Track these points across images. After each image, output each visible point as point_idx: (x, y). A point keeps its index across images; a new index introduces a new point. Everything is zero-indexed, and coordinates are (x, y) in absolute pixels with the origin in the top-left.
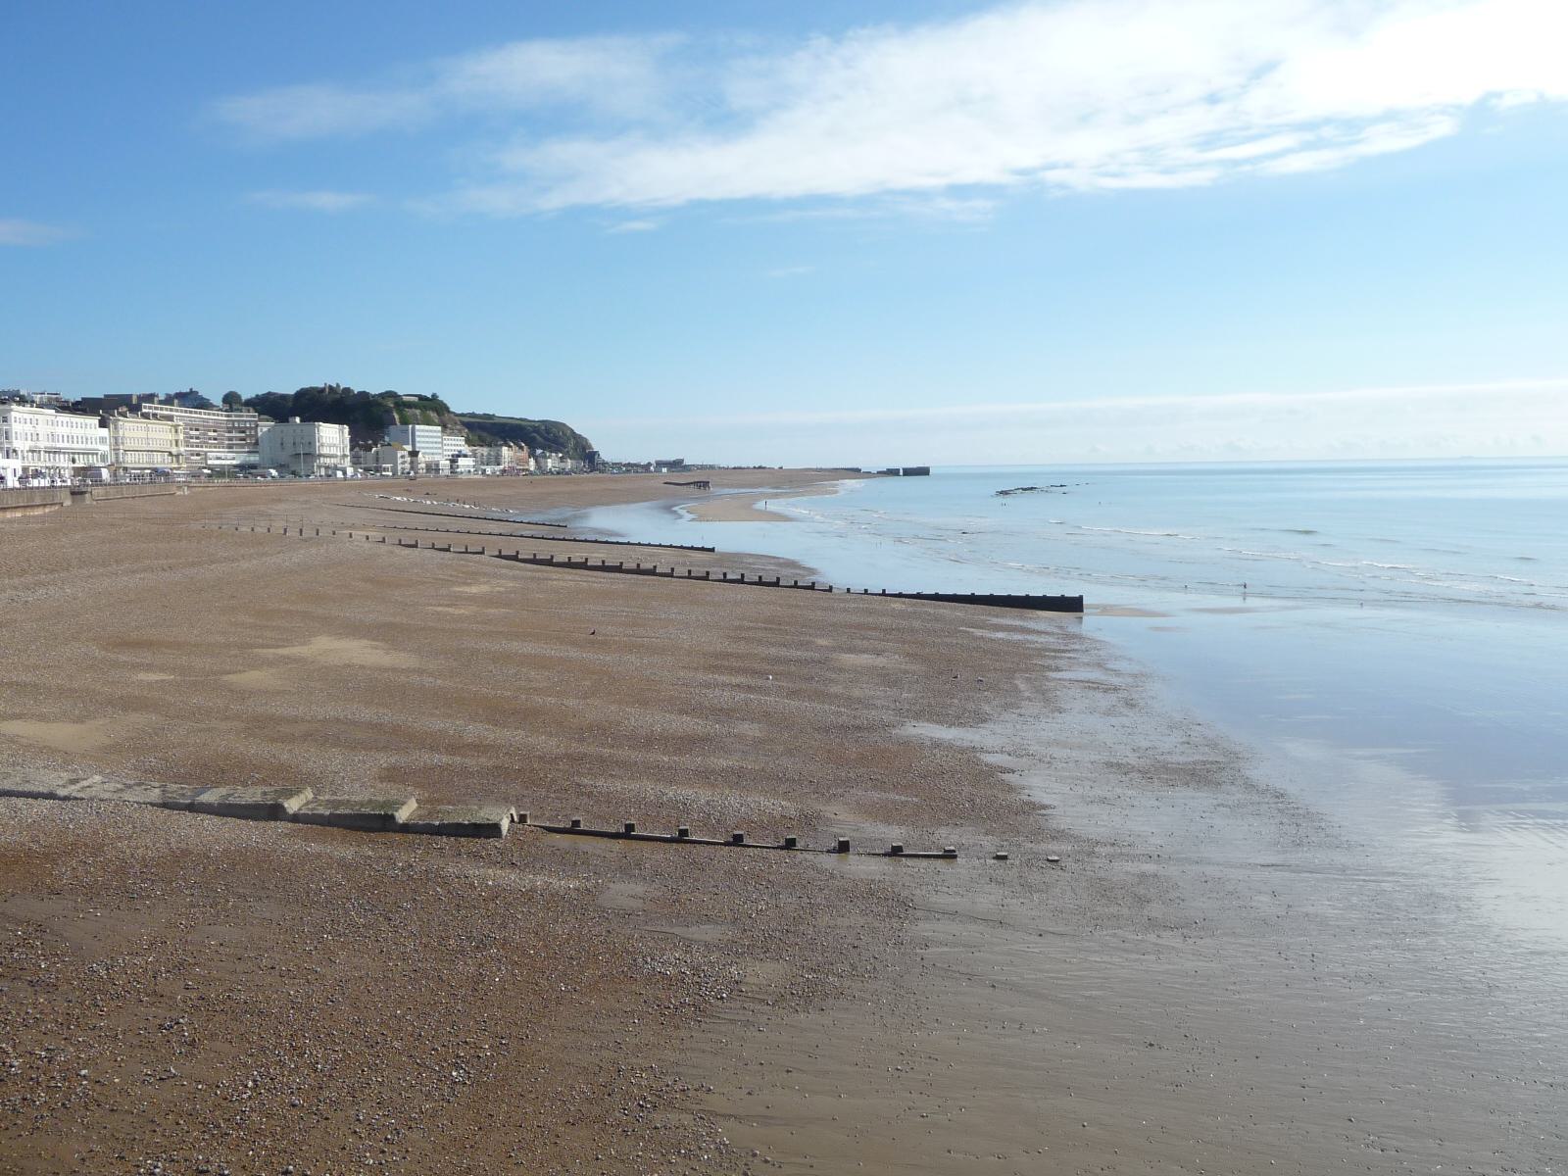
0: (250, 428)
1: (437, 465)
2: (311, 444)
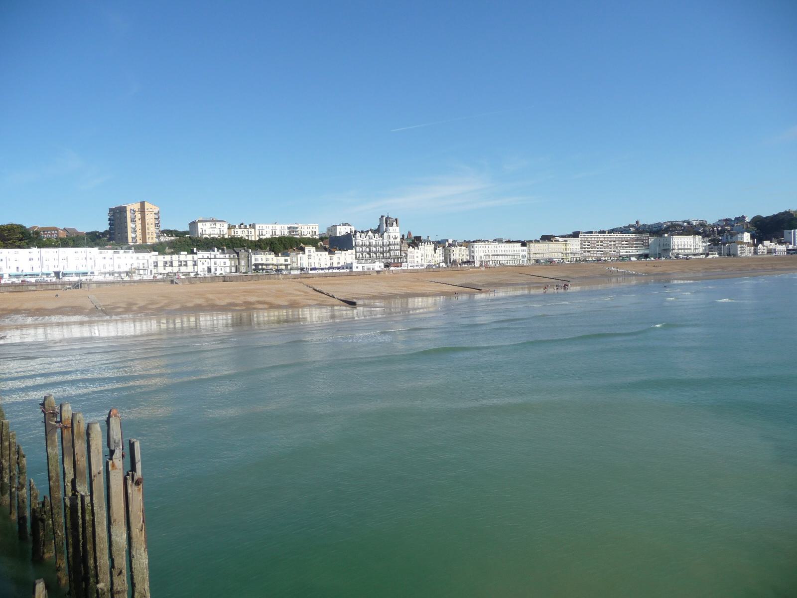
0: (646, 240)
1: (775, 250)
2: (669, 245)
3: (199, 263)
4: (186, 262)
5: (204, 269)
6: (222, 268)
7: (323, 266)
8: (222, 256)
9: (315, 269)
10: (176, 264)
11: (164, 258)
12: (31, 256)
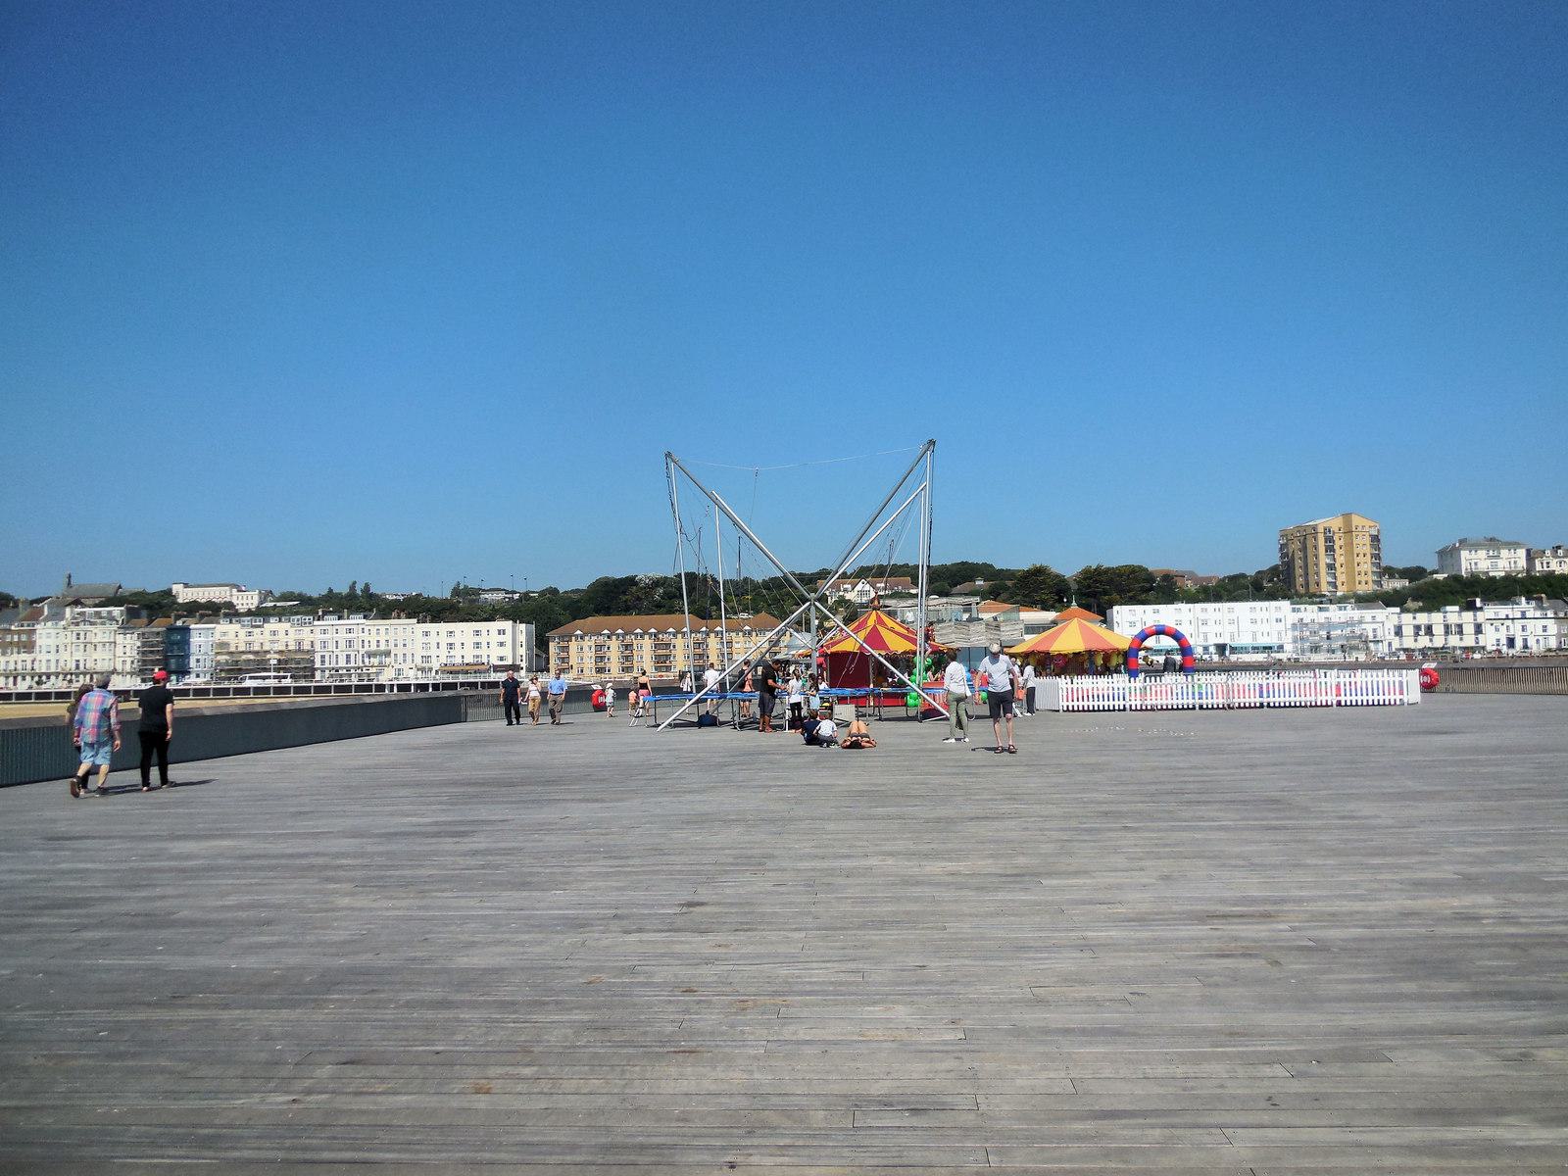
3: (1487, 628)
4: (1460, 626)
5: (1498, 640)
6: (1540, 638)
8: (1538, 614)
10: (1438, 630)
11: (1414, 618)
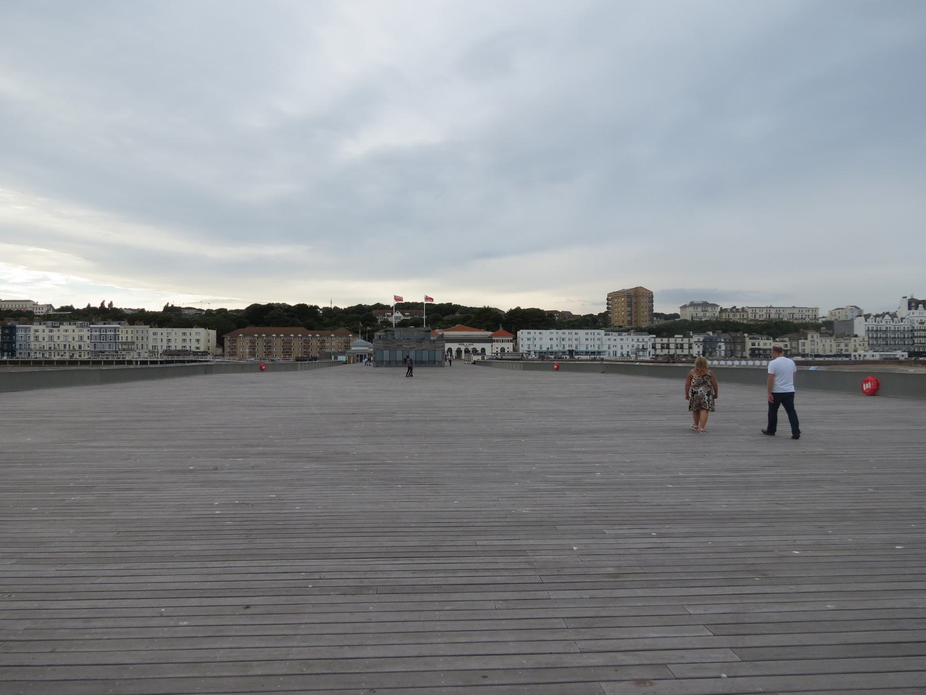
7: (828, 353)
9: (817, 356)
12: (551, 336)
